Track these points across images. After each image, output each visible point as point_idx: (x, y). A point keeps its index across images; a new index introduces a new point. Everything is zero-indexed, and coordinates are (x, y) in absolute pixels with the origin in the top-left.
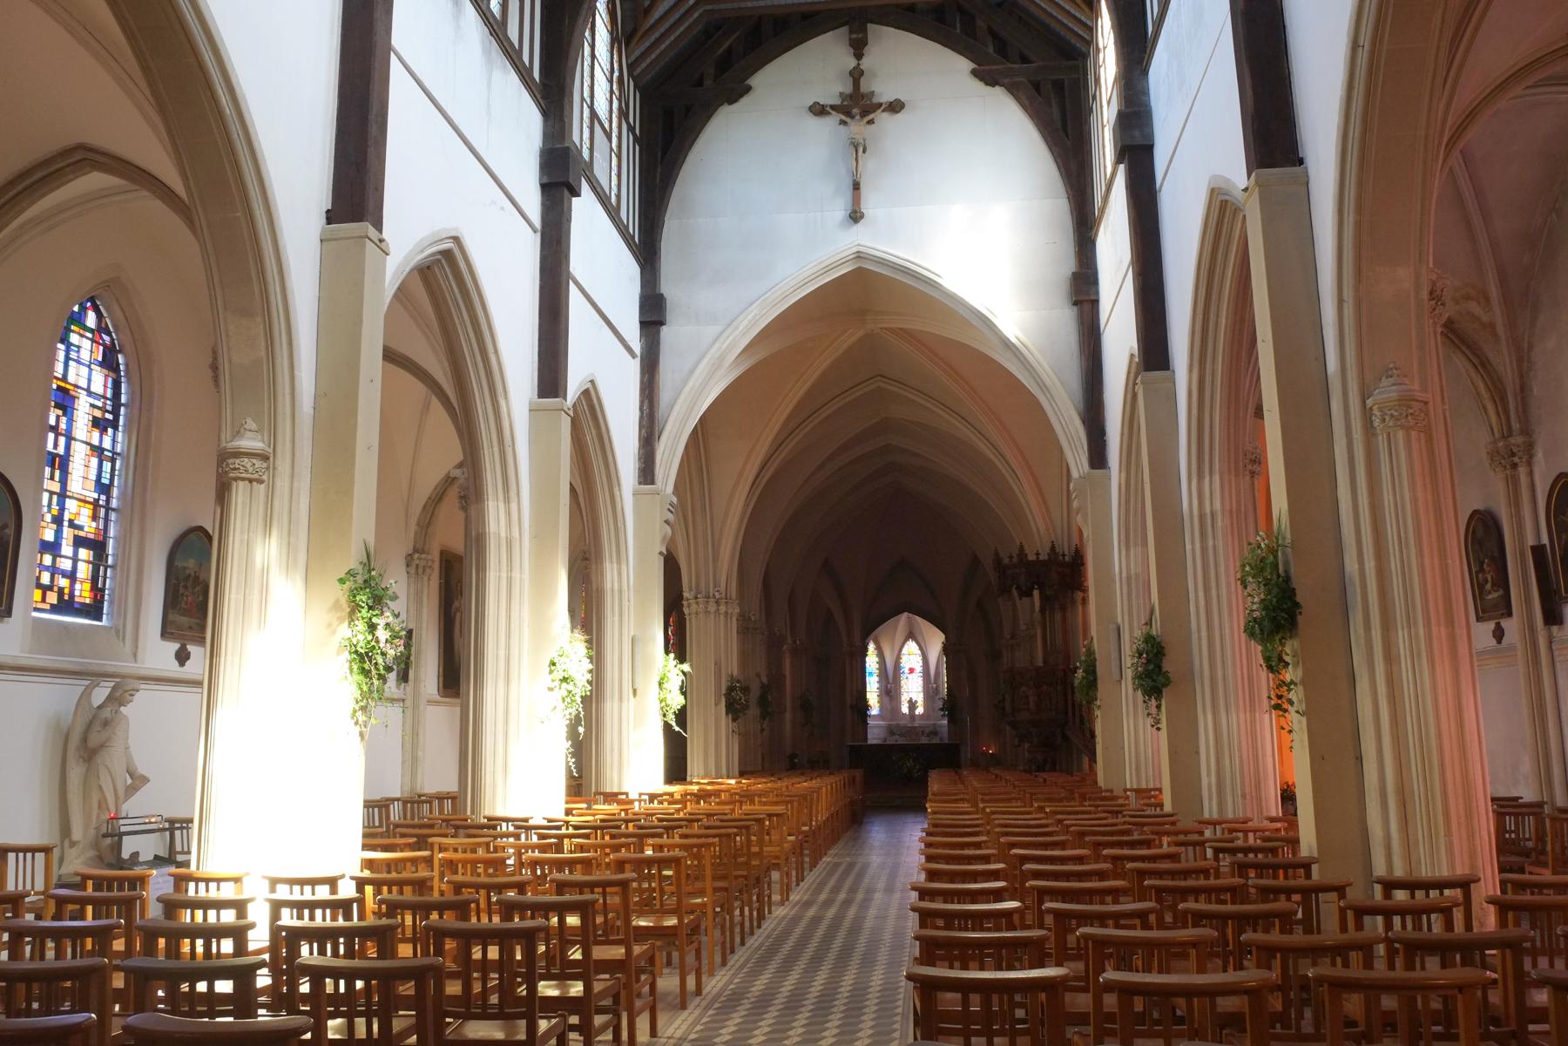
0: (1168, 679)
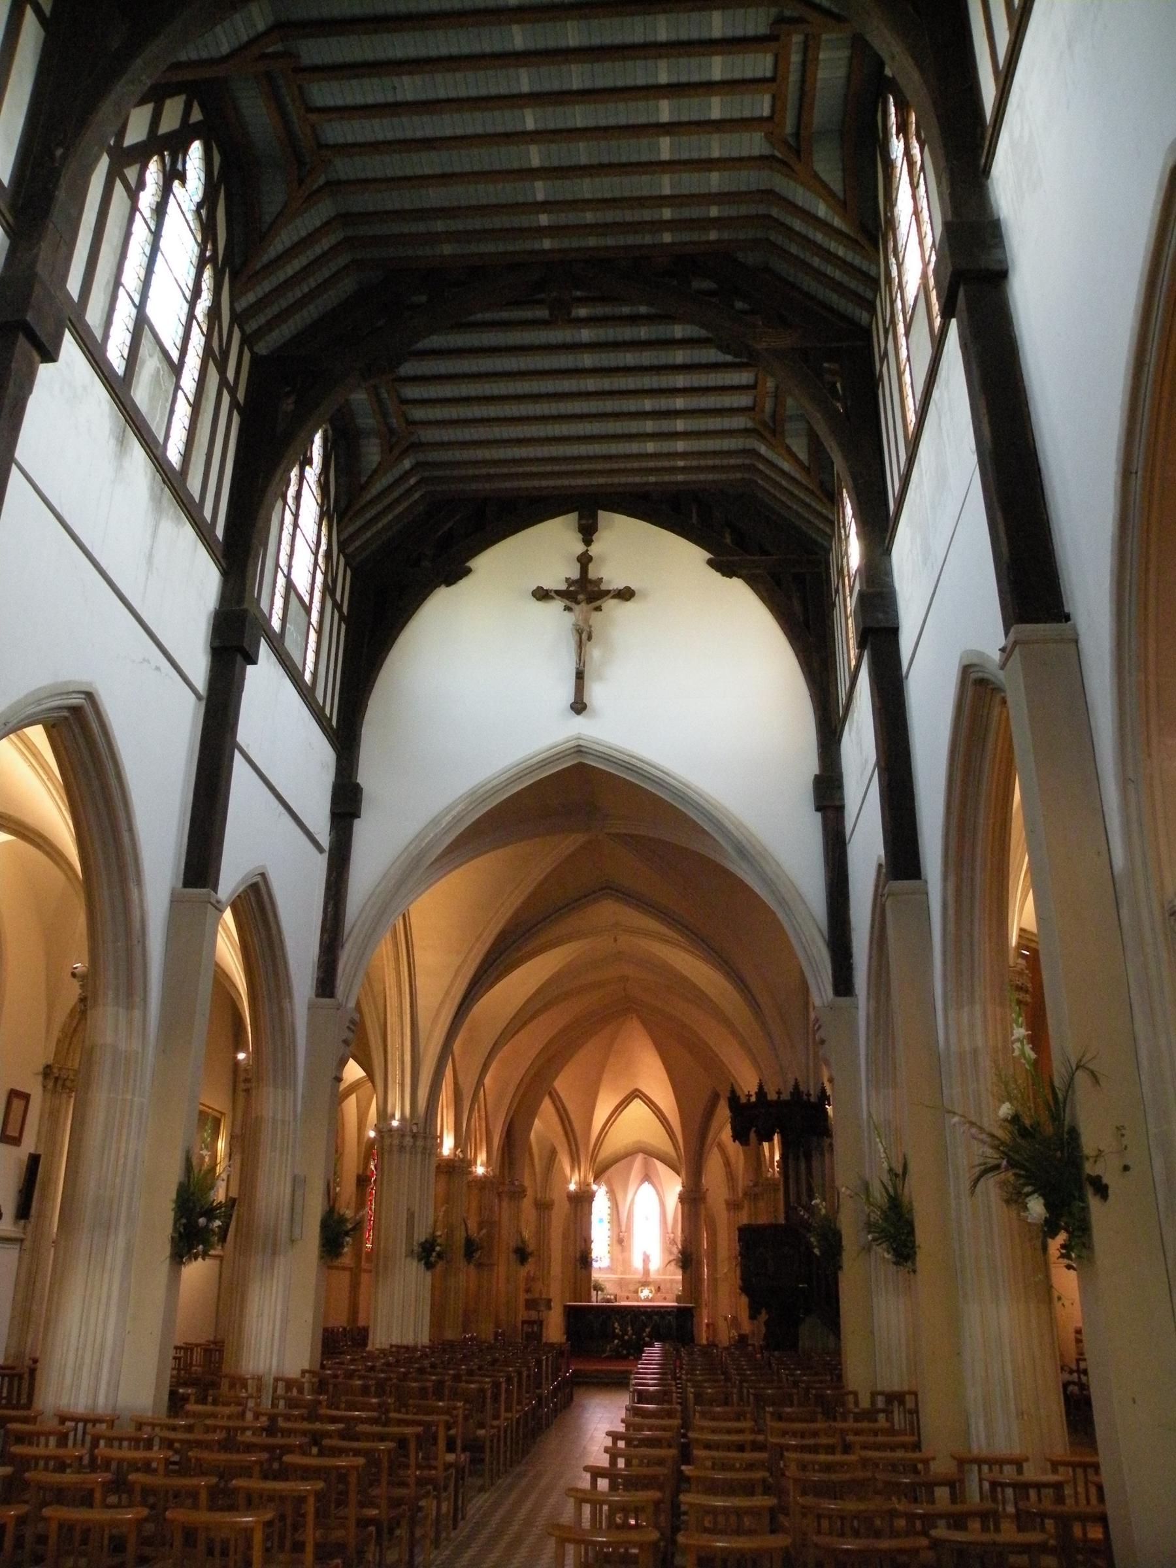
0: (895, 1398)
